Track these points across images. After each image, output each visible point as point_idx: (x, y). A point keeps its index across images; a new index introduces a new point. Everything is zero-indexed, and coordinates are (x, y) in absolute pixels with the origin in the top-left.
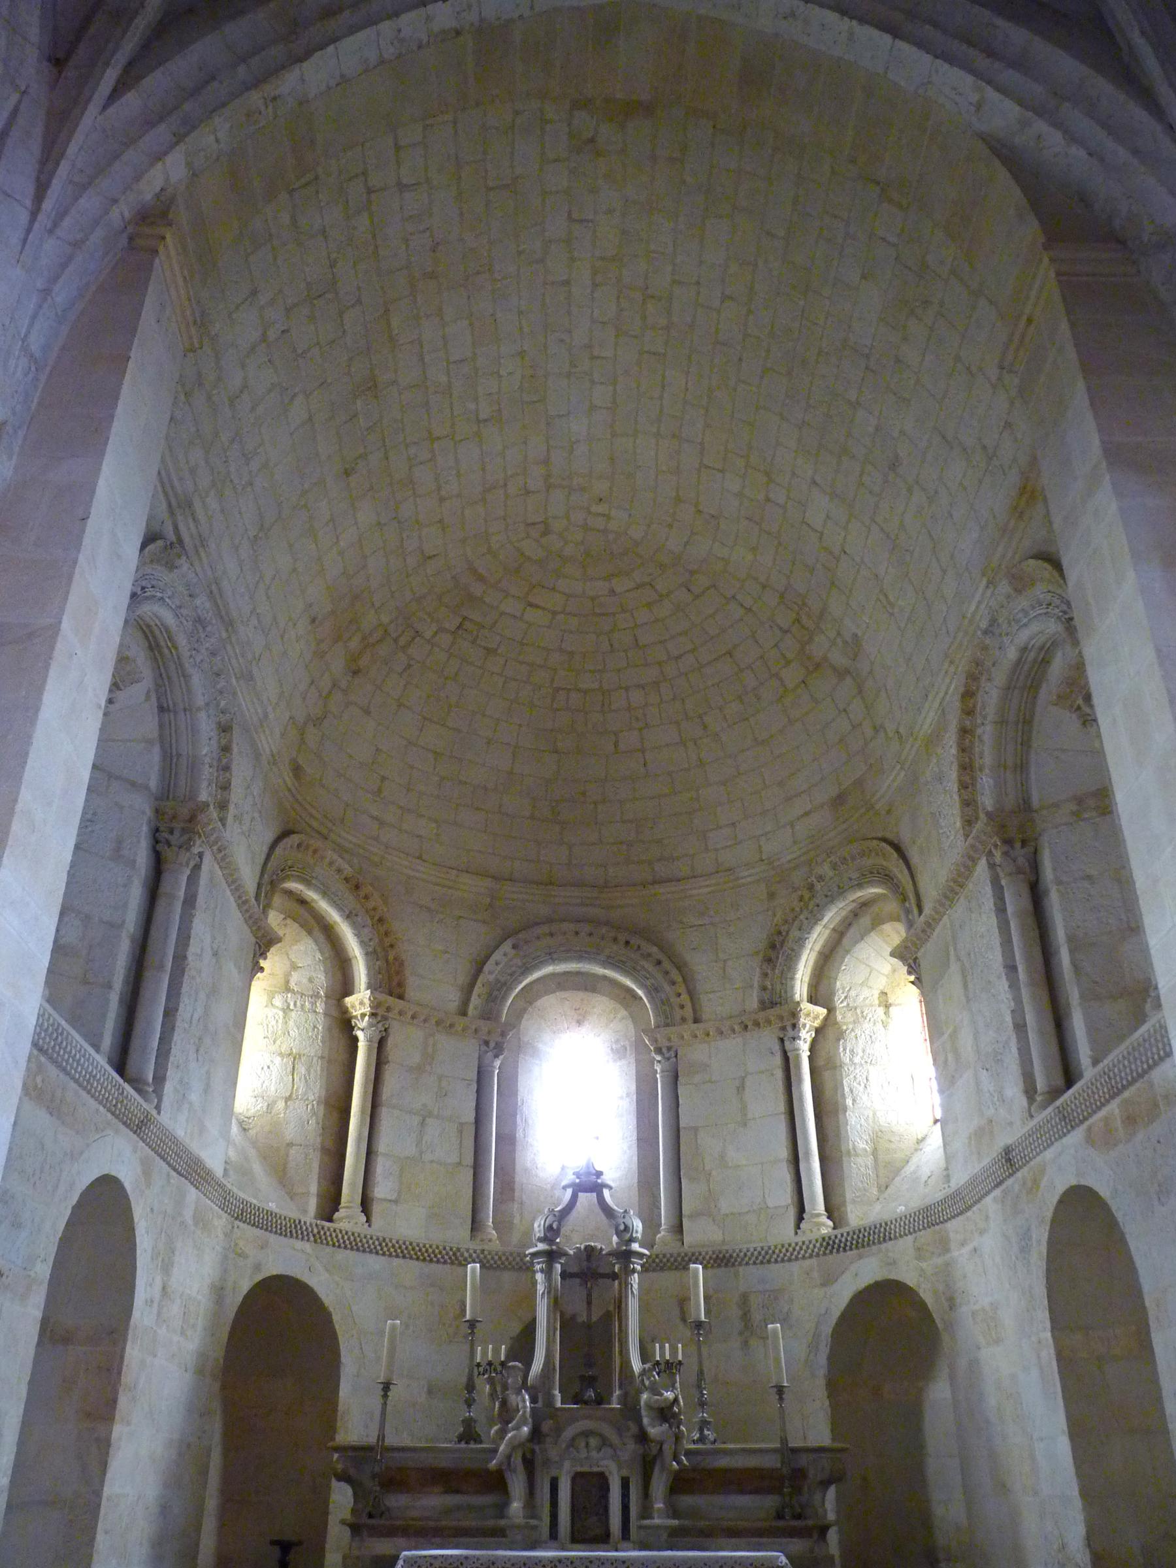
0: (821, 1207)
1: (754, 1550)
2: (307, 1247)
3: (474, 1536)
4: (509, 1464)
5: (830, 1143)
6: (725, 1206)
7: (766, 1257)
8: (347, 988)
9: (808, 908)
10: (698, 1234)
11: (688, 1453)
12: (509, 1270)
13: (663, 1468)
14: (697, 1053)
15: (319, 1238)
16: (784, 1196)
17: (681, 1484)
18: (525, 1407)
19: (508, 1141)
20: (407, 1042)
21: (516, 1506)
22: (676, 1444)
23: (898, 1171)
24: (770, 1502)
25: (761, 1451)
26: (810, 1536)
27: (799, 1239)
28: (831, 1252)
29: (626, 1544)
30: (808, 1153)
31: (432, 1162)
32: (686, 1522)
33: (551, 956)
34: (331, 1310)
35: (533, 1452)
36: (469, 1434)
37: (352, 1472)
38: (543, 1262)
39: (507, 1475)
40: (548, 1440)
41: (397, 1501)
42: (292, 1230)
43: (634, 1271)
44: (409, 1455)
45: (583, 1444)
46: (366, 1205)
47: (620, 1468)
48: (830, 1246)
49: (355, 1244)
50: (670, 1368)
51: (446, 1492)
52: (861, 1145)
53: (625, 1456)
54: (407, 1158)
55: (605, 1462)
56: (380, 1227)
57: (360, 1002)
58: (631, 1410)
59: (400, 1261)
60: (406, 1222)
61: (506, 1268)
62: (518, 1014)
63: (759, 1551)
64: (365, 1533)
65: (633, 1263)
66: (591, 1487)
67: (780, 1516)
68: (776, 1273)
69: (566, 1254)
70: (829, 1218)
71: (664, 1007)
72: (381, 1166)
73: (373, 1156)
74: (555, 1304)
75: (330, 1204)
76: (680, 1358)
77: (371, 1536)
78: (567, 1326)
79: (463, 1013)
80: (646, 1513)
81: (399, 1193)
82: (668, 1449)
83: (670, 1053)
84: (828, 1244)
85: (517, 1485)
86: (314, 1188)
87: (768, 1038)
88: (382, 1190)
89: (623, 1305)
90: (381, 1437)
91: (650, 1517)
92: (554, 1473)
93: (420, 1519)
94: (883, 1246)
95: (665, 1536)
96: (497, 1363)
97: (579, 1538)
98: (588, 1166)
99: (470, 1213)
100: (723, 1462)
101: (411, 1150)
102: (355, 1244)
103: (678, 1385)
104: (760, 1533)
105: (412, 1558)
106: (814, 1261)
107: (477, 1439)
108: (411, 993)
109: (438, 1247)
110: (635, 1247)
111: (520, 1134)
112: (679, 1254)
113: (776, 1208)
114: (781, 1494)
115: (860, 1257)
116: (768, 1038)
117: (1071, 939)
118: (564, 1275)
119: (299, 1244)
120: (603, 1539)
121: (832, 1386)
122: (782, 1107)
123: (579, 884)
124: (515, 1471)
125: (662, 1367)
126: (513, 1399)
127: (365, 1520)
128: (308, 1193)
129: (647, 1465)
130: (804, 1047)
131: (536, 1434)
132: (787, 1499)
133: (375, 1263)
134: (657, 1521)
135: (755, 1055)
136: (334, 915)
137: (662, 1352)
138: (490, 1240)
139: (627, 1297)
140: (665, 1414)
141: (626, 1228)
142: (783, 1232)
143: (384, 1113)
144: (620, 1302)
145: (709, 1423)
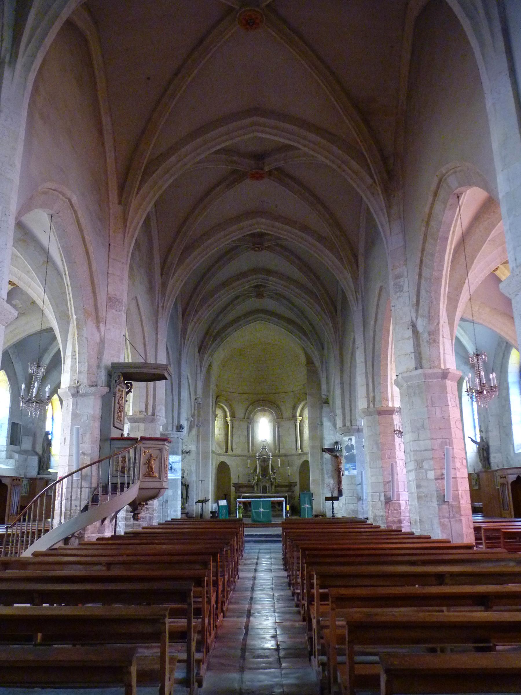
7: (292, 455)
8: (226, 416)
9: (299, 401)
10: (282, 452)
14: (282, 423)
15: (227, 455)
16: (294, 447)
17: (276, 487)
19: (253, 437)
20: (236, 424)
21: (255, 489)
24: (287, 488)
33: (258, 407)
36: (249, 481)
41: (241, 489)
48: (300, 454)
49: (232, 456)
57: (229, 419)
58: (270, 478)
60: (238, 452)
62: (253, 416)
66: (265, 488)
71: (277, 415)
72: (234, 444)
74: (260, 465)
75: (226, 452)
78: (261, 467)
79: (244, 418)
83: (278, 423)
85: (255, 487)
87: (293, 422)
88: (234, 447)
97: (263, 493)
102: (232, 456)
108: (236, 416)
116: (293, 422)
117: (250, 503)
120: (266, 493)
121: (300, 474)
122: (294, 433)
123: (263, 394)
129: (272, 485)
130: (298, 424)
131: (258, 481)
135: (290, 424)
136: (224, 406)
137: (274, 471)
140: (274, 478)
142: (294, 452)
143: (234, 436)
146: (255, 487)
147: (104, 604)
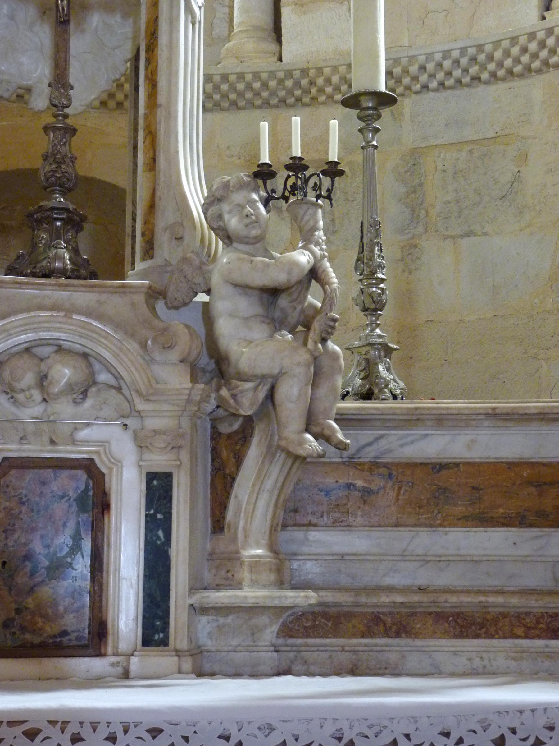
11: (343, 420)
22: (315, 385)
27: (547, 24)
32: (329, 597)
45: (29, 378)
47: (142, 443)
50: (293, 183)
53: (160, 418)
80: (221, 566)
82: (292, 395)
89: (163, 39)
95: (270, 634)
103: (320, 234)
129: (223, 452)
134: (250, 594)
139: (173, 21)
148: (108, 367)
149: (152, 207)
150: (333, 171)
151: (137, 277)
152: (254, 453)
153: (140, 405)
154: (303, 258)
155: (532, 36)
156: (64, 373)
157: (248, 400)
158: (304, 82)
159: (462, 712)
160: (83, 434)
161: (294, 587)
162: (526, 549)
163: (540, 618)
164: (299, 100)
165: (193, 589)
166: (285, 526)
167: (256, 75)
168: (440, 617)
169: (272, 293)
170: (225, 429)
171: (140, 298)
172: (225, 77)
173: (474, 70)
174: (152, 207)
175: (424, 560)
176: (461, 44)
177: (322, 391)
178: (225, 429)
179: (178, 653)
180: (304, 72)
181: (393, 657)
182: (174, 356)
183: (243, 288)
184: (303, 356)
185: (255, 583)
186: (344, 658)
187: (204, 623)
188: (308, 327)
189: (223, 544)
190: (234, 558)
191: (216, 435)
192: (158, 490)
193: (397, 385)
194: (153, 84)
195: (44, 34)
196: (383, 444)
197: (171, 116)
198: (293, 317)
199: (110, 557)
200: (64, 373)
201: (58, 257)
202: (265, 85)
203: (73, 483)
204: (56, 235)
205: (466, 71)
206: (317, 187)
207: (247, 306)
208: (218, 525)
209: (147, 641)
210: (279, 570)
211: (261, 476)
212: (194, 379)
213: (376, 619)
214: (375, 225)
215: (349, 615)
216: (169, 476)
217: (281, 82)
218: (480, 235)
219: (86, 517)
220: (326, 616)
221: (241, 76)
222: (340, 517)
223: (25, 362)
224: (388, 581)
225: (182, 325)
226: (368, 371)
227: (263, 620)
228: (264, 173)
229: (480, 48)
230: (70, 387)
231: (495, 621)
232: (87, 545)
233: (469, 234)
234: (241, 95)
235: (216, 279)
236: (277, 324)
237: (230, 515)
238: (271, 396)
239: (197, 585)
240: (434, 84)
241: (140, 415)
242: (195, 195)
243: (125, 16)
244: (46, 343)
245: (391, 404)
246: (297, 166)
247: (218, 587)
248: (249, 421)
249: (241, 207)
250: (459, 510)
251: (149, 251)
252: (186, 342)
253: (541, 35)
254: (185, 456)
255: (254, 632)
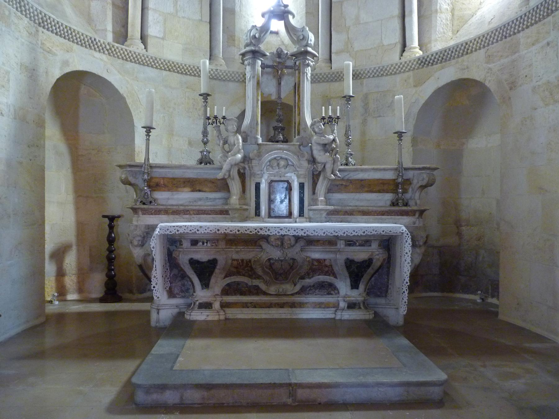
0: (416, 43)
1: (378, 223)
2: (104, 57)
3: (210, 214)
4: (229, 176)
5: (424, 7)
6: (357, 46)
11: (340, 171)
12: (232, 81)
13: (325, 178)
16: (396, 38)
18: (239, 143)
21: (234, 199)
22: (333, 164)
23: (466, 22)
24: (388, 197)
25: (384, 170)
26: (414, 215)
27: (401, 61)
28: (423, 66)
29: (302, 219)
30: (411, 12)
31: (184, 17)
32: (336, 207)
34: (125, 95)
35: (244, 168)
36: (205, 160)
37: (131, 179)
38: (249, 58)
39: (229, 182)
40: (254, 161)
41: (162, 196)
42: (91, 44)
43: (308, 65)
44: (167, 170)
45: (276, 164)
46: (143, 39)
47: (298, 177)
48: (423, 62)
50: (330, 121)
51: (192, 191)
52: (445, 6)
53: (302, 172)
54: (169, 14)
55: (288, 175)
56: (152, 51)
59: (168, 73)
60: (172, 52)
61: (230, 80)
63: (381, 223)
64: (140, 213)
65: (308, 60)
67: (393, 204)
68: (386, 82)
69: (264, 55)
70: (420, 49)
72: (151, 16)
73: (146, 11)
75: (122, 35)
76: (338, 115)
77: (144, 214)
80: (314, 201)
81: (165, 33)
82: (329, 167)
84: (422, 62)
85: (235, 186)
86: (110, 27)
88: (153, 30)
89: (301, 86)
90: (147, 159)
91: (316, 205)
92: (258, 180)
93: (176, 205)
94: (460, 60)
95: (324, 215)
96: (220, 117)
98: (279, 5)
99: (209, 50)
100: (361, 176)
101: (171, 9)
103: (335, 131)
104: (383, 213)
105: (165, 227)
106: (411, 73)
107: (210, 162)
109: (190, 66)
110: (310, 49)
111: (237, 9)
112: (329, 73)
113: (388, 45)
114: (397, 193)
115: (443, 68)
118: (263, 66)
119: (97, 54)
124: (233, 179)
125: (326, 121)
126: (231, 139)
127: (139, 205)
128: (106, 30)
129: (315, 177)
132: (400, 195)
133: (151, 72)
134: (320, 207)
138: (221, 65)
139: (304, 81)
140: (326, 147)
141: (304, 38)
142: (394, 57)
144: (299, 84)
145: (351, 155)
146: (235, 186)
147: (404, 315)
148: (291, 162)
149: (299, 124)
150: (338, 118)
151: (296, 141)
152: (321, 178)
153: (298, 169)
154: (331, 137)
155: (397, 64)
156: (282, 163)
157: (320, 168)
158: (338, 75)
159: (357, 227)
160: (287, 175)
161: (329, 205)
162: (380, 198)
163: (380, 212)
164: (336, 80)
165: (309, 206)
166: (328, 193)
167: (325, 74)
168: (359, 212)
169: (325, 145)
170: (315, 173)
171: (297, 147)
172: (317, 75)
173: (382, 73)
174: (299, 124)
175: (358, 200)
176: (378, 66)
177: (335, 165)
178: (315, 173)
179: (306, 218)
180: (338, 73)
181: (349, 219)
182: (305, 159)
183: (319, 144)
184: (331, 159)
185: (321, 205)
186: (339, 220)
187: (311, 212)
188: (332, 151)
189: (315, 197)
190: (317, 200)
191: (313, 174)
192: (302, 186)
193: (353, 163)
194: (299, 96)
195: (274, 82)
196: (349, 175)
197: (303, 104)
198: (330, 149)
199: (292, 200)
200: (282, 163)
201: (280, 138)
202: (327, 76)
203: (285, 185)
204: (279, 133)
205: (380, 73)
206: (335, 121)
207: (319, 148)
208: (314, 193)
209: (300, 216)
210: (326, 202)
211: (323, 183)
212: (309, 164)
213: (346, 212)
214: (349, 126)
215: (341, 211)
216: (303, 183)
217: (331, 75)
218: (273, 245)
219: (287, 192)
220: (336, 211)
221: (321, 74)
222: (340, 191)
223: (275, 161)
224: (350, 204)
225: (306, 150)
226: (347, 159)
227: (323, 212)
228: (323, 118)
229: (383, 67)
230: (284, 166)
231: (370, 212)
232: (288, 198)
233: (380, 116)
234: (321, 79)
235: (313, 142)
236: (326, 151)
237: (316, 191)
238: (324, 167)
239: (310, 205)
240: (372, 76)
241: (298, 171)
242: (309, 122)
243: (292, 76)
244: (278, 157)
245: (351, 167)
246: (330, 117)
247: (314, 205)
248: (320, 172)
249: (318, 127)
250: (366, 189)
251: (299, 134)
252: (307, 156)
253: (399, 64)
254: (307, 179)
255: (321, 214)
